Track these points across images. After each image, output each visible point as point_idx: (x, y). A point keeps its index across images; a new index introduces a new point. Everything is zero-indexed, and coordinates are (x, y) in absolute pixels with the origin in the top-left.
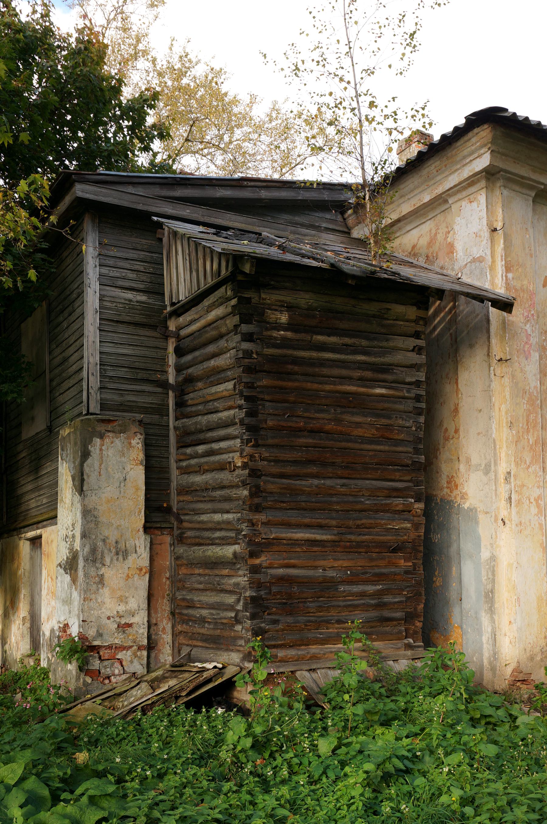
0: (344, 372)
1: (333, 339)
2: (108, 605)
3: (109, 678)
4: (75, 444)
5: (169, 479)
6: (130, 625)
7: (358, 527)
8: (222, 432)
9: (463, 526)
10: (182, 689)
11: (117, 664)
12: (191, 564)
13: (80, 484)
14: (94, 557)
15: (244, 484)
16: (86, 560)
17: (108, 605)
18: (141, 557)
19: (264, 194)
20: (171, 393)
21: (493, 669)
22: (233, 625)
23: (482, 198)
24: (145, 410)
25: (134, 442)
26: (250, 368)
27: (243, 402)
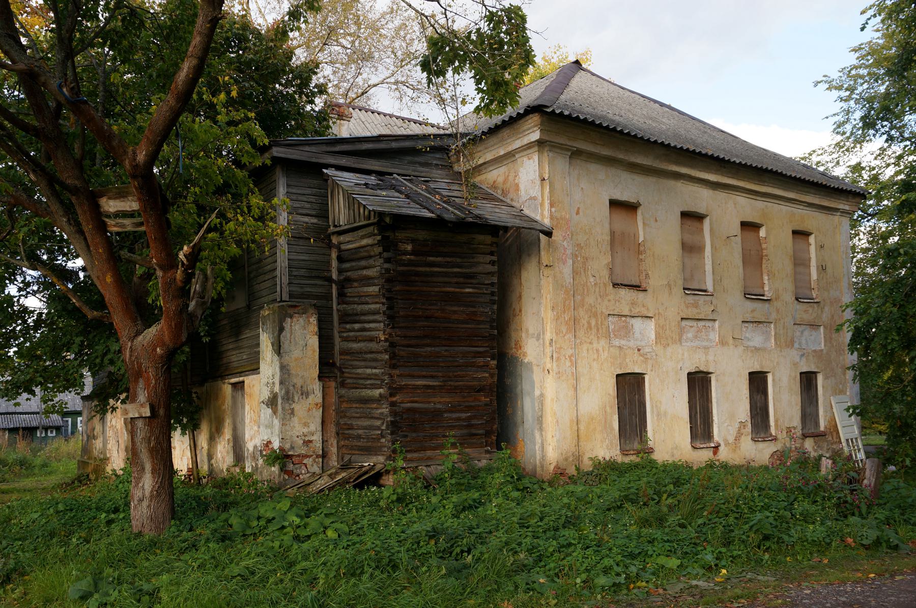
0: (446, 279)
1: (439, 259)
2: (297, 429)
3: (298, 476)
4: (274, 322)
5: (333, 344)
6: (311, 441)
7: (455, 376)
8: (371, 318)
9: (525, 374)
10: (350, 478)
11: (303, 467)
12: (350, 401)
13: (278, 348)
14: (288, 397)
15: (386, 351)
16: (283, 399)
17: (297, 428)
18: (317, 397)
19: (394, 145)
20: (334, 285)
21: (542, 466)
22: (379, 439)
23: (536, 157)
24: (317, 297)
25: (311, 320)
26: (389, 280)
27: (385, 301)
